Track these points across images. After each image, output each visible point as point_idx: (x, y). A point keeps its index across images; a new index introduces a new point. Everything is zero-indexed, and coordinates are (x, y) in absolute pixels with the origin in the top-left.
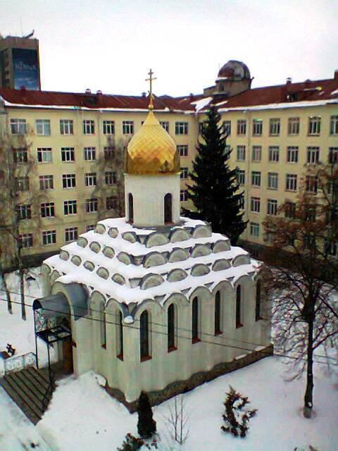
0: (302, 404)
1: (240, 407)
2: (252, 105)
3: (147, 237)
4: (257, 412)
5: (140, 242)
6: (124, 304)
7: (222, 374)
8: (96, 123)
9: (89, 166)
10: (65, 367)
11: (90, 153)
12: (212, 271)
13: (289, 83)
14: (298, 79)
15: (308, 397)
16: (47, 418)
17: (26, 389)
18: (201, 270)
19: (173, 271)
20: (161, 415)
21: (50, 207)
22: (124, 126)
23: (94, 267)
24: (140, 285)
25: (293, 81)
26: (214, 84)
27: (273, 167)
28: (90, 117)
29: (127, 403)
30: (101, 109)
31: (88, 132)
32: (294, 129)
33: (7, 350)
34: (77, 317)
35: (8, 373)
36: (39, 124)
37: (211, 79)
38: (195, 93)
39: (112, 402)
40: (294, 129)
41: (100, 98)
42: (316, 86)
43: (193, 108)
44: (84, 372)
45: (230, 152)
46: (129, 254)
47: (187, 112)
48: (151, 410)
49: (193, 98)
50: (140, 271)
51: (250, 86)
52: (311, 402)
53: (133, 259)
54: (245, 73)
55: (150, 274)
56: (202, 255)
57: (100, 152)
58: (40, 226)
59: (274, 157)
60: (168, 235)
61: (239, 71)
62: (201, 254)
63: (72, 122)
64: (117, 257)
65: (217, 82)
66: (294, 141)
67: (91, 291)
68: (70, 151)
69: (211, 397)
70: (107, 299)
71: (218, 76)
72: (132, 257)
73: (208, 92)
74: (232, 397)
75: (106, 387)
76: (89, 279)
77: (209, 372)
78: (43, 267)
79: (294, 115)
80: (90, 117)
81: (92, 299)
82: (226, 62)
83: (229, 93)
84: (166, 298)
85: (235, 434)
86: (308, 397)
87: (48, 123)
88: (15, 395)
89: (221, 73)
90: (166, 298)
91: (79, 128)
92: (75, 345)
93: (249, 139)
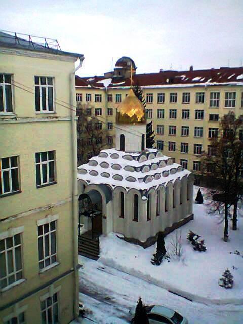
1: (196, 239)
3: (139, 157)
6: (141, 191)
7: (169, 233)
10: (97, 229)
13: (161, 72)
15: (226, 233)
16: (101, 255)
19: (156, 174)
24: (144, 181)
26: (113, 71)
27: (185, 123)
31: (98, 101)
32: (173, 99)
34: (107, 202)
37: (111, 67)
38: (98, 75)
40: (173, 99)
42: (181, 75)
43: (102, 85)
44: (110, 232)
46: (133, 166)
47: (101, 88)
48: (164, 241)
49: (97, 78)
51: (74, 66)
53: (135, 169)
55: (147, 176)
62: (162, 166)
65: (114, 69)
66: (173, 106)
67: (113, 188)
69: (184, 232)
70: (127, 190)
72: (135, 167)
75: (125, 239)
76: (110, 181)
79: (186, 91)
81: (115, 192)
84: (157, 187)
86: (226, 233)
89: (118, 64)
90: (157, 187)
92: (105, 218)
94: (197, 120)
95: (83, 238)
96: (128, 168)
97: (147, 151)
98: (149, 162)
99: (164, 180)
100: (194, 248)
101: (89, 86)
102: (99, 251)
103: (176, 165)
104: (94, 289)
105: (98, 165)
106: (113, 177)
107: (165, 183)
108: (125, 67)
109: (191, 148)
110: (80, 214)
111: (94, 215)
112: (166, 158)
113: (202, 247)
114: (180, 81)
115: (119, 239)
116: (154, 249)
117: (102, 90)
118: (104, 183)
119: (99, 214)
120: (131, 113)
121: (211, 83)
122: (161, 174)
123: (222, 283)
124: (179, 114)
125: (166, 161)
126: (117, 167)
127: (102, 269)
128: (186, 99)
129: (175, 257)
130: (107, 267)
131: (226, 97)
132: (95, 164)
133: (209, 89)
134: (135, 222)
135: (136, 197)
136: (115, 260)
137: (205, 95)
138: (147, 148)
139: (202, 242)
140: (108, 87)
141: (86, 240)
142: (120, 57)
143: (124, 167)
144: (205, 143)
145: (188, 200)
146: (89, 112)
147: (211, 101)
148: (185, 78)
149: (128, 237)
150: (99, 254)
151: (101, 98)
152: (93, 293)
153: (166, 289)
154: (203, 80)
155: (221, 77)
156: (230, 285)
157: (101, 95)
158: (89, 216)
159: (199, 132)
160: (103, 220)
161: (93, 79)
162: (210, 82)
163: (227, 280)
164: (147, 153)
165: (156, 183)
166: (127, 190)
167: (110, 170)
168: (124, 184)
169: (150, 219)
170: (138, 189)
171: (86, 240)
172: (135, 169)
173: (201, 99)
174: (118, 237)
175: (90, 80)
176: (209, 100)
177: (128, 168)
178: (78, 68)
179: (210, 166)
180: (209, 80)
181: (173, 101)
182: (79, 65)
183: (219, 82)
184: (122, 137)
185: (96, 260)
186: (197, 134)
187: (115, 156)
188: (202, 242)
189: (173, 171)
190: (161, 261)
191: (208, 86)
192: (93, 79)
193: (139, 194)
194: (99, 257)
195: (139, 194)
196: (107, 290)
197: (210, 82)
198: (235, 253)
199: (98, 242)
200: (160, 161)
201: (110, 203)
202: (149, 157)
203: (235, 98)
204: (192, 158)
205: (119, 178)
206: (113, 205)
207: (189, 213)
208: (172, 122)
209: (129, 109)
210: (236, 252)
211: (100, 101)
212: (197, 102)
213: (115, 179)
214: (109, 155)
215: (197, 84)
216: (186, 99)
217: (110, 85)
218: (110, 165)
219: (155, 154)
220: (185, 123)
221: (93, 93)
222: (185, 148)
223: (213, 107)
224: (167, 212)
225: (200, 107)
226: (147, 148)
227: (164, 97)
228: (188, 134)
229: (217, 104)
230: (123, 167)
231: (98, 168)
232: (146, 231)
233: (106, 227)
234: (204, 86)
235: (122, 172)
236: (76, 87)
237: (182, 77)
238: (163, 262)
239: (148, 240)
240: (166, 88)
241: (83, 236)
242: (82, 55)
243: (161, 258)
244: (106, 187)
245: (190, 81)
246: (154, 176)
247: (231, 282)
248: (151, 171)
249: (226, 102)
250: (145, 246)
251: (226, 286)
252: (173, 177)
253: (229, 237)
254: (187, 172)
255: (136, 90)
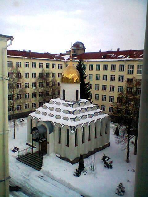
0: (126, 158)
1: (107, 160)
2: (89, 59)
3: (73, 105)
4: (113, 162)
5: (70, 106)
6: (71, 127)
8: (29, 63)
9: (33, 80)
10: (44, 151)
11: (34, 75)
12: (93, 117)
13: (100, 51)
14: (104, 50)
15: (128, 156)
16: (43, 168)
17: (30, 160)
18: (90, 116)
19: (83, 116)
20: (86, 162)
21: (28, 95)
22: (40, 65)
23: (54, 115)
24: (74, 120)
25: (102, 51)
27: (113, 83)
28: (27, 61)
29: (71, 161)
30: (32, 58)
32: (105, 68)
33: (14, 149)
34: (50, 133)
35: (19, 156)
36: (9, 63)
38: (62, 53)
39: (64, 162)
40: (105, 68)
41: (30, 53)
43: (63, 59)
44: (51, 153)
45: (86, 76)
47: (62, 60)
49: (61, 55)
50: (73, 116)
52: (129, 157)
54: (83, 47)
55: (76, 117)
56: (89, 111)
57: (38, 75)
58: (24, 102)
59: (98, 78)
60: (78, 104)
61: (81, 46)
62: (89, 111)
63: (20, 62)
64: (63, 111)
66: (105, 73)
67: (55, 124)
68: (122, 77)
69: (99, 156)
70: (63, 126)
71: (73, 47)
72: (69, 111)
73: (68, 53)
74: (105, 157)
75: (61, 158)
76: (53, 120)
77: (93, 151)
78: (28, 117)
80: (27, 61)
81: (55, 126)
82: (76, 42)
83: (77, 54)
84: (83, 125)
85: (109, 168)
86: (128, 156)
87: (11, 63)
88: (26, 163)
89: (74, 46)
90: (83, 125)
91: (31, 65)
92: (49, 143)
93: (31, 70)
94: (108, 81)
95: (34, 155)
96: (65, 111)
97: (80, 100)
98: (80, 108)
99: (89, 120)
100: (105, 166)
101: (55, 59)
102: (42, 165)
103: (99, 110)
104: (32, 190)
105: (48, 109)
106: (55, 117)
107: (89, 122)
108: (78, 48)
109: (108, 99)
110: (33, 140)
111: (41, 141)
112: (92, 105)
113: (110, 165)
114: (110, 57)
115: (57, 157)
116: (77, 166)
117: (63, 61)
118: (49, 121)
119: (45, 140)
120: (70, 76)
121: (129, 59)
122: (87, 116)
123: (117, 192)
124: (109, 78)
125: (92, 108)
126: (58, 110)
127: (42, 177)
128: (113, 68)
129: (90, 172)
130: (45, 176)
131: (138, 68)
132: (46, 108)
133: (127, 62)
134: (67, 147)
135: (68, 130)
136: (50, 172)
137: (125, 66)
138: (80, 98)
139: (112, 162)
140: (67, 60)
141: (36, 157)
142: (75, 42)
143: (63, 110)
144: (116, 95)
145: (106, 133)
146: (48, 75)
147: (128, 70)
148: (114, 55)
149: (62, 156)
150: (41, 167)
151: (62, 66)
152: (30, 193)
153: (79, 193)
154: (124, 57)
155: (135, 55)
156: (122, 193)
157: (62, 65)
158: (38, 142)
159: (112, 89)
160: (48, 144)
161: (59, 55)
162: (128, 58)
163: (120, 190)
164: (79, 102)
165: (82, 121)
166: (63, 126)
167: (54, 112)
168: (61, 122)
169: (84, 143)
170: (69, 126)
171: (36, 157)
172: (70, 112)
173: (122, 69)
174: (57, 156)
175: (58, 55)
176: (137, 70)
177: (65, 111)
178: (9, 45)
179: (118, 111)
180: (128, 57)
181: (105, 70)
182: (10, 43)
183: (134, 58)
184: (64, 91)
185: (39, 171)
186: (111, 90)
187: (58, 103)
188: (112, 162)
189: (95, 114)
190: (80, 174)
191: (127, 60)
192: (59, 55)
193: (70, 129)
194: (41, 169)
195: (70, 129)
196: (40, 192)
197: (112, 55)
198: (131, 171)
199: (42, 159)
200: (88, 108)
201: (52, 133)
202: (80, 105)
203: (133, 68)
204: (108, 104)
205: (58, 117)
206: (54, 136)
207: (107, 142)
208: (104, 83)
209: (68, 74)
210: (133, 170)
211: (62, 68)
212: (120, 71)
213: (57, 118)
214: (55, 103)
215: (120, 59)
216: (113, 68)
217: (68, 59)
218: (55, 109)
219: (85, 103)
220: (113, 83)
221: (57, 63)
222: (104, 98)
223: (97, 70)
224: (90, 141)
225: (122, 73)
226: (80, 98)
227: (100, 67)
228: (114, 91)
229: (132, 72)
230: (62, 110)
231: (48, 111)
232: (73, 152)
233: (49, 149)
234: (124, 60)
235: (62, 114)
236: (8, 57)
237: (112, 54)
238: (81, 174)
239: (75, 159)
240: (101, 62)
241: (34, 154)
242: (12, 37)
243: (81, 172)
244: (50, 123)
245: (116, 58)
246: (82, 117)
247: (124, 192)
248: (80, 114)
249: (138, 71)
250: (73, 163)
251: (120, 194)
252: (95, 118)
253: (130, 159)
254: (106, 115)
255: (80, 62)
